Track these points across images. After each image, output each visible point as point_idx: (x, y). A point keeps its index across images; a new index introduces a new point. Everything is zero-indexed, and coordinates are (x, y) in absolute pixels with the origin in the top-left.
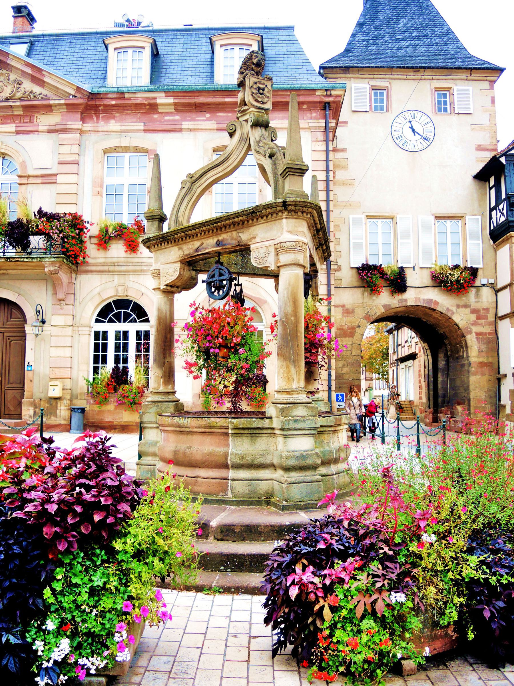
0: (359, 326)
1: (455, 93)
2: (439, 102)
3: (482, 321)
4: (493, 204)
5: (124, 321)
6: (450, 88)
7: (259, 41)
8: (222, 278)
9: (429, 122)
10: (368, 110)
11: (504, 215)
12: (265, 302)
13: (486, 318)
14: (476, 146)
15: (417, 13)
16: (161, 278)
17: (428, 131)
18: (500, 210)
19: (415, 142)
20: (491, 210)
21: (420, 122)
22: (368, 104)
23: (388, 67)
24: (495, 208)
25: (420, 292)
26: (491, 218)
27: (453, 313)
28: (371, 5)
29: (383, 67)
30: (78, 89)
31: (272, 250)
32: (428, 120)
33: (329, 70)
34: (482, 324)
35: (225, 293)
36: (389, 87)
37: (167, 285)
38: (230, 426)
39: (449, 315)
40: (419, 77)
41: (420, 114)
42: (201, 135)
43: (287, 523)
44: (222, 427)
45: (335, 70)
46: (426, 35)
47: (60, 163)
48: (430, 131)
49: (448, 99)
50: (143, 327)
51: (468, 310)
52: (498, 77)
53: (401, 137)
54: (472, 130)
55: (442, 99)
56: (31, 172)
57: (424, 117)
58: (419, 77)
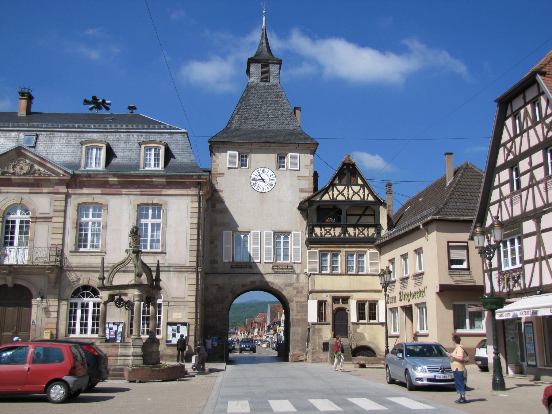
0: (227, 297)
13: (302, 292)
15: (274, 100)
17: (271, 180)
27: (282, 289)
28: (246, 95)
30: (66, 172)
32: (272, 173)
41: (268, 170)
42: (132, 197)
47: (55, 211)
48: (273, 180)
50: (97, 300)
51: (291, 288)
54: (298, 179)
56: (38, 215)
57: (270, 171)
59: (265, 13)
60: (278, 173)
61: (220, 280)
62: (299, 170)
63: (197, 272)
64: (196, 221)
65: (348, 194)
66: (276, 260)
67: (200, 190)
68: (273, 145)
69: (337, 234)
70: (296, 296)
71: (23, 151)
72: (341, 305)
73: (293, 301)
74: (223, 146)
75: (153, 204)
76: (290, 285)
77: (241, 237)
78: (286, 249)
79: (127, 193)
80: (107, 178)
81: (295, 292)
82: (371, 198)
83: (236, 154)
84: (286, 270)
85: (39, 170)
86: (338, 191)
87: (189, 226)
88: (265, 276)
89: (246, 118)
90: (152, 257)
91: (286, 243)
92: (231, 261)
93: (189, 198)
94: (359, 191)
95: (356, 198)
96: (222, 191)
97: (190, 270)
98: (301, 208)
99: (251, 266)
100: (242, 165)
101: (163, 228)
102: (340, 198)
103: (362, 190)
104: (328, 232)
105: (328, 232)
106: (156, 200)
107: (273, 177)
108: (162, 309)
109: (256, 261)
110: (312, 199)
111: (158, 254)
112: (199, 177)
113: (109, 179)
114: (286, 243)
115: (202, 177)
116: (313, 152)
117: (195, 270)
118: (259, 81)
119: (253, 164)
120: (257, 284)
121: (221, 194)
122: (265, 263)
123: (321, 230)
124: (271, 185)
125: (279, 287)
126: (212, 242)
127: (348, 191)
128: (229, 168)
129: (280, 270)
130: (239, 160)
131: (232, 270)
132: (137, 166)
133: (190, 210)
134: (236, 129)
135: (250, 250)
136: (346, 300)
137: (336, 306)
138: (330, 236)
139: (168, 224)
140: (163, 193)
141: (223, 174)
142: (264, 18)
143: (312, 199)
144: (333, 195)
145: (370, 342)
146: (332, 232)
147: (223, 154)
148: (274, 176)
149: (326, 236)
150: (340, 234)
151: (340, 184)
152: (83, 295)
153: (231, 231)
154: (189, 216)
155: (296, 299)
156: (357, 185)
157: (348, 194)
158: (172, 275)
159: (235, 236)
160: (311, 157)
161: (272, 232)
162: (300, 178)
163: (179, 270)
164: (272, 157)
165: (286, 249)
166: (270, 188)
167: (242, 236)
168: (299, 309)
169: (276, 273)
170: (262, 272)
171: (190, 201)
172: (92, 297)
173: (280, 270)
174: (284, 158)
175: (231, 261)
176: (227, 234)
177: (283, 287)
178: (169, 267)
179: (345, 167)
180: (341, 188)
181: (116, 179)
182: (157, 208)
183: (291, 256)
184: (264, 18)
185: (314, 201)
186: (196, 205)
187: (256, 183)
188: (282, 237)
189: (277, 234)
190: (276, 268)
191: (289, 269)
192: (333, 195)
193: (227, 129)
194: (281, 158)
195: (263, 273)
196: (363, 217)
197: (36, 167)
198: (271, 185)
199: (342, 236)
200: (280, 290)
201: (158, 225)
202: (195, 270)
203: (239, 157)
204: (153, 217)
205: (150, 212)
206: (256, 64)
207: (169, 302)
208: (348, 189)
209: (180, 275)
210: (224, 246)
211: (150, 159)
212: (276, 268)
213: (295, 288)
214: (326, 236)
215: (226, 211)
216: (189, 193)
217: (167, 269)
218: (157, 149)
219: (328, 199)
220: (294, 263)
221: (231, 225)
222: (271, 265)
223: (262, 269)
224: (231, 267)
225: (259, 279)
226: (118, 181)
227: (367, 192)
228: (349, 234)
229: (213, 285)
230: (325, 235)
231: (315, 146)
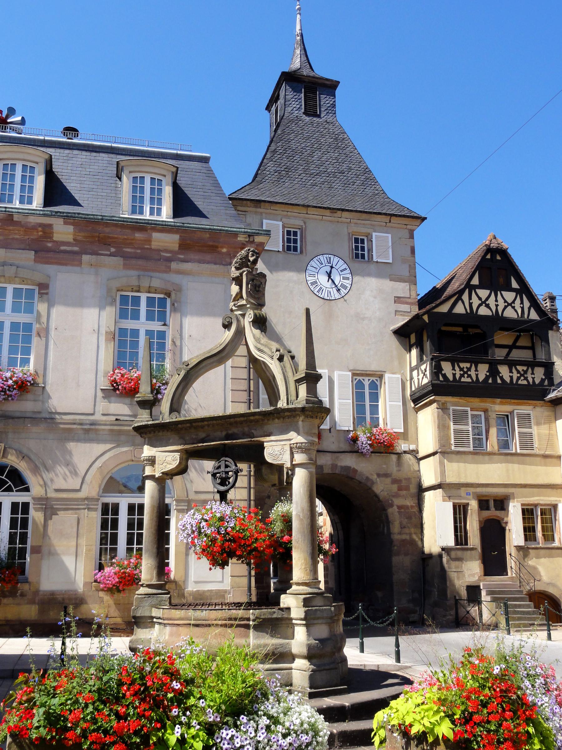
0: (269, 497)
1: (374, 240)
2: (357, 248)
3: (404, 493)
4: (414, 363)
6: (369, 234)
7: (173, 172)
9: (345, 269)
11: (427, 377)
13: (407, 488)
16: (156, 466)
18: (422, 371)
20: (412, 370)
22: (281, 244)
23: (304, 206)
24: (417, 368)
25: (337, 458)
26: (411, 378)
27: (373, 483)
29: (298, 205)
31: (287, 448)
32: (345, 266)
33: (238, 201)
34: (403, 495)
36: (304, 226)
37: (162, 473)
38: (252, 617)
39: (369, 484)
40: (336, 219)
41: (336, 259)
43: (325, 706)
44: (242, 619)
45: (245, 202)
49: (366, 245)
50: (21, 498)
51: (388, 480)
52: (418, 226)
53: (316, 282)
55: (360, 245)
57: (341, 262)
65: (497, 306)
69: (482, 378)
70: (397, 496)
72: (492, 513)
73: (392, 505)
74: (254, 209)
76: (386, 475)
81: (395, 487)
82: (534, 316)
86: (480, 299)
94: (513, 302)
95: (510, 313)
102: (483, 311)
103: (518, 300)
104: (466, 373)
105: (465, 373)
123: (454, 369)
125: (367, 478)
127: (496, 301)
136: (501, 504)
137: (486, 514)
138: (469, 380)
144: (471, 304)
145: (548, 584)
146: (473, 373)
149: (463, 380)
150: (487, 378)
151: (481, 286)
155: (398, 502)
156: (511, 289)
157: (497, 306)
161: (350, 374)
168: (405, 521)
172: (9, 489)
179: (488, 257)
180: (483, 293)
187: (316, 282)
192: (471, 304)
196: (511, 344)
199: (490, 381)
208: (496, 296)
213: (395, 481)
214: (463, 380)
219: (462, 311)
225: (330, 463)
227: (527, 304)
228: (501, 378)
230: (460, 378)
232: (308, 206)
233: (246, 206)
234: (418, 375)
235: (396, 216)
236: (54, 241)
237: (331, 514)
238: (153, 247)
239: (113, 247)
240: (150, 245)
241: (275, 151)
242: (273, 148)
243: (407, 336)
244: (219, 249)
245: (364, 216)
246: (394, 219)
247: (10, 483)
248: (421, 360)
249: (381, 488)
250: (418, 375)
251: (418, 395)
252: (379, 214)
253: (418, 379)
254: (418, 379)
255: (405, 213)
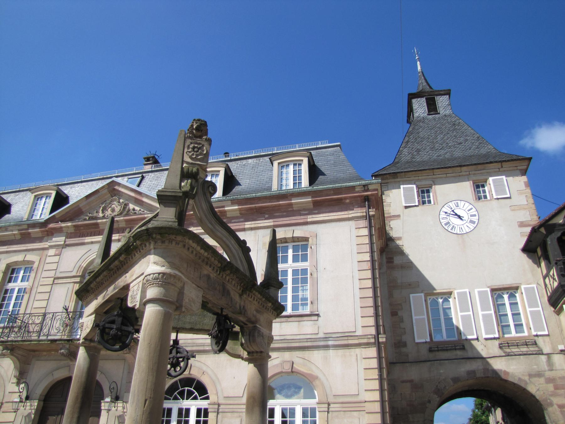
0: (429, 402)
4: (545, 272)
5: (187, 399)
8: (179, 355)
10: (417, 204)
11: (556, 281)
12: (316, 378)
14: (519, 223)
17: (472, 216)
18: (551, 276)
19: (462, 226)
20: (544, 278)
21: (464, 209)
26: (546, 285)
27: (526, 383)
32: (471, 206)
35: (182, 369)
40: (458, 174)
41: (463, 203)
45: (385, 176)
46: (460, 143)
48: (475, 215)
50: (203, 404)
51: (542, 380)
53: (448, 223)
57: (467, 204)
58: (458, 174)
59: (418, 59)
60: (480, 204)
61: (414, 373)
62: (510, 198)
63: (378, 344)
64: (367, 257)
66: (503, 334)
67: (369, 208)
68: (464, 169)
70: (554, 395)
71: (116, 187)
73: (551, 404)
74: (393, 180)
75: (294, 239)
77: (438, 303)
78: (516, 315)
79: (253, 226)
80: (224, 207)
81: (551, 387)
83: (413, 187)
84: (524, 349)
85: (134, 210)
87: (356, 266)
88: (491, 361)
89: (418, 151)
90: (296, 324)
91: (514, 305)
92: (428, 340)
93: (352, 223)
96: (400, 239)
97: (365, 341)
98: (528, 249)
99: (463, 346)
100: (424, 203)
101: (311, 274)
106: (299, 232)
107: (473, 212)
108: (317, 419)
109: (469, 337)
110: (551, 222)
111: (305, 318)
112: (365, 187)
113: (226, 208)
114: (514, 305)
115: (371, 187)
116: (524, 172)
117: (373, 340)
118: (426, 114)
119: (439, 198)
120: (478, 375)
121: (399, 242)
122: (486, 339)
124: (472, 222)
125: (520, 379)
126: (394, 314)
128: (406, 207)
129: (515, 350)
130: (418, 196)
131: (431, 356)
132: (270, 188)
133: (355, 241)
134: (408, 162)
135: (458, 321)
139: (320, 267)
140: (309, 220)
141: (399, 216)
142: (418, 63)
143: (551, 222)
147: (395, 191)
148: (474, 210)
152: (182, 394)
153: (423, 295)
154: (355, 251)
155: (556, 401)
158: (331, 352)
159: (429, 302)
160: (524, 179)
161: (489, 290)
162: (514, 208)
163: (345, 343)
164: (467, 187)
165: (516, 315)
166: (472, 226)
167: (441, 301)
169: (508, 355)
170: (484, 354)
171: (354, 227)
172: (195, 398)
173: (514, 350)
174: (483, 186)
175: (428, 340)
176: (416, 300)
177: (527, 378)
178: (326, 339)
181: (237, 207)
182: (302, 245)
183: (528, 324)
184: (418, 63)
185: (555, 225)
186: (365, 232)
188: (506, 296)
189: (497, 292)
190: (507, 347)
191: (530, 347)
193: (394, 163)
194: (479, 186)
195: (485, 356)
197: (131, 206)
198: (472, 222)
200: (523, 385)
201: (304, 271)
202: (373, 340)
203: (418, 192)
204: (295, 259)
205: (290, 252)
206: (419, 99)
207: (329, 404)
209: (347, 351)
210: (414, 318)
211: (287, 179)
212: (507, 347)
213: (549, 380)
215: (409, 266)
216: (350, 216)
217: (322, 343)
218: (298, 164)
220: (537, 336)
221: (421, 284)
222: (497, 343)
223: (482, 349)
224: (431, 350)
225: (481, 367)
226: (240, 210)
229: (403, 382)
231: (526, 163)
232: (433, 169)
233: (387, 179)
234: (550, 281)
235: (504, 161)
236: (228, 218)
237: (505, 415)
238: (294, 209)
239: (267, 214)
240: (292, 208)
241: (408, 142)
242: (407, 139)
243: (535, 251)
244: (344, 201)
245: (480, 167)
246: (504, 164)
247: (196, 393)
248: (549, 269)
249: (536, 388)
250: (550, 281)
251: (554, 298)
252: (491, 162)
253: (550, 284)
254: (550, 284)
255: (515, 158)
